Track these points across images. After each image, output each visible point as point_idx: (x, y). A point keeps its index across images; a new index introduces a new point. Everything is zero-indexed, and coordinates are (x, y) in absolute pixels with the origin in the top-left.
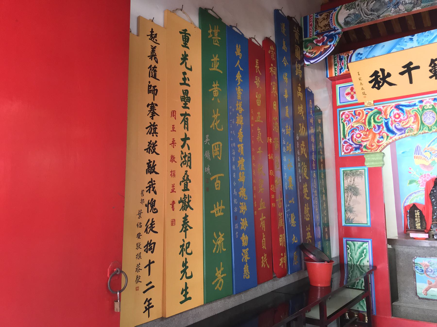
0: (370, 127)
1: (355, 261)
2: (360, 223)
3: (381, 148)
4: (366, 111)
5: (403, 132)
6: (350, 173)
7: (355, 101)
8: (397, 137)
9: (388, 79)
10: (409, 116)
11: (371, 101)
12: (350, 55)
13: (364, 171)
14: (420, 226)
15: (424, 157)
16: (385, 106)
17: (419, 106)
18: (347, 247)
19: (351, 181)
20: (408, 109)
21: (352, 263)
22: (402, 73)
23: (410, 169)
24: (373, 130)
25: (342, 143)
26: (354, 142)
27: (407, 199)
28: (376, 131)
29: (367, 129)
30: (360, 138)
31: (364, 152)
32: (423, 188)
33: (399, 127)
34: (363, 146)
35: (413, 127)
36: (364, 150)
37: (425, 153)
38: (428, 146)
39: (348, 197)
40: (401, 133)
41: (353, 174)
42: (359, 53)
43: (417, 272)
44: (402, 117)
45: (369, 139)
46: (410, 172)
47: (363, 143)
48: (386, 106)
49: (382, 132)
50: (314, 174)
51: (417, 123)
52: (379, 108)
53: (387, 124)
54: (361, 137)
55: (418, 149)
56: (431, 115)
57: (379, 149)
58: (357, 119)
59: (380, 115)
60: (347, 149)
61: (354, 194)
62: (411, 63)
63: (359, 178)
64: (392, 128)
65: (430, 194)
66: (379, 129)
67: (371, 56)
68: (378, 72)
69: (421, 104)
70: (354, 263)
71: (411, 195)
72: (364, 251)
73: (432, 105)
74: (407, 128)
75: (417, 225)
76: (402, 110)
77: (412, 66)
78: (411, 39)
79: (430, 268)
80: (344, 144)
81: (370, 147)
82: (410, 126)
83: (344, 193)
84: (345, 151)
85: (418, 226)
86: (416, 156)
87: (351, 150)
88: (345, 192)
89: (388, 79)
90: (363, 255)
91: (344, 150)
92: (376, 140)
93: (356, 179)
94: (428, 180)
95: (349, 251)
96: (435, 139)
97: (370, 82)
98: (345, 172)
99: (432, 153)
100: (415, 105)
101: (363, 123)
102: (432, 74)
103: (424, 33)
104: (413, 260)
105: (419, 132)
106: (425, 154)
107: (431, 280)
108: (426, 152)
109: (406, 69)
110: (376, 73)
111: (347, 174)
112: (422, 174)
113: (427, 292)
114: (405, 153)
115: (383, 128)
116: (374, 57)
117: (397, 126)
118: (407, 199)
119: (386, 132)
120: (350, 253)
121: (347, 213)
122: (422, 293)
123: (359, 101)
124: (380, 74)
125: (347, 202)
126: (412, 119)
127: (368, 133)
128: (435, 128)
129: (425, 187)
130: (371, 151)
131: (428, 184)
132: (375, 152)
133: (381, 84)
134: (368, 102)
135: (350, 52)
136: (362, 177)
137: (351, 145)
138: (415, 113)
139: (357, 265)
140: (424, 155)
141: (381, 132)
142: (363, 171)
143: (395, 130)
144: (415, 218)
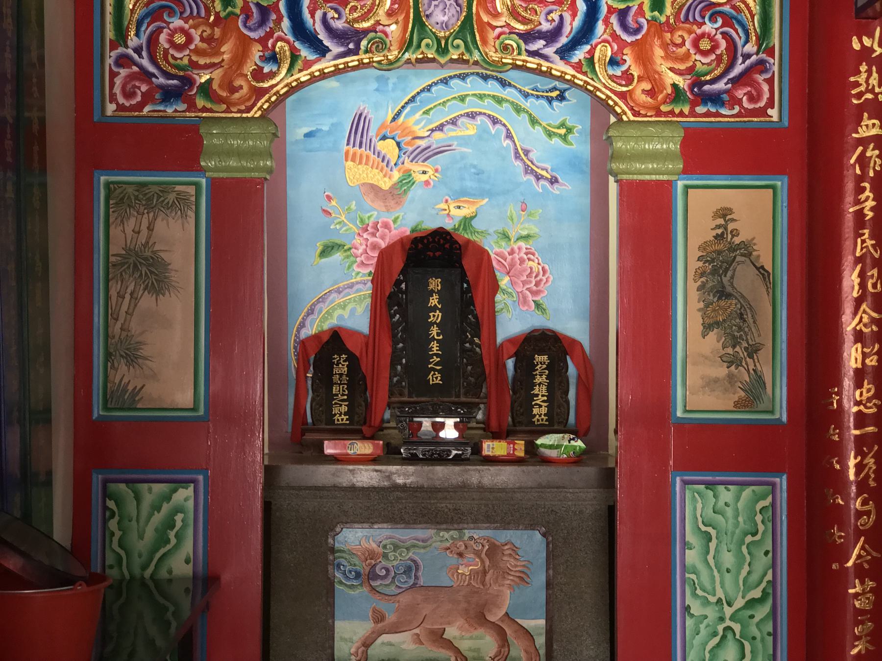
0: (230, 9)
1: (137, 562)
2: (165, 407)
3: (266, 101)
6: (137, 198)
8: (327, 64)
13: (193, 193)
15: (376, 156)
18: (105, 508)
19: (139, 232)
21: (123, 575)
23: (329, 198)
25: (109, 61)
26: (163, 63)
27: (311, 312)
28: (250, 29)
29: (217, 14)
30: (187, 52)
32: (364, 275)
33: (339, 25)
34: (198, 84)
35: (388, 30)
36: (200, 102)
37: (382, 141)
38: (394, 119)
39: (121, 296)
40: (342, 49)
41: (150, 199)
43: (341, 583)
45: (223, 60)
47: (198, 74)
49: (276, 35)
50: (10, 187)
51: (401, 18)
54: (192, 47)
55: (359, 123)
57: (259, 104)
60: (128, 89)
61: (147, 285)
63: (170, 219)
64: (314, 23)
65: (390, 297)
66: (263, 22)
70: (129, 573)
71: (322, 299)
72: (174, 521)
74: (366, 32)
75: (335, 410)
79: (384, 563)
80: (115, 69)
81: (224, 94)
83: (107, 281)
84: (121, 100)
85: (340, 413)
87: (147, 98)
88: (113, 278)
90: (172, 534)
91: (115, 94)
92: (248, 65)
93: (160, 225)
94: (383, 245)
95: (113, 524)
96: (418, 93)
98: (115, 189)
99: (402, 145)
104: (330, 541)
105: (407, 56)
106: (381, 146)
107: (383, 606)
108: (384, 138)
111: (122, 199)
112: (367, 222)
113: (368, 651)
114: (314, 136)
117: (333, 18)
118: (311, 312)
119: (290, 38)
120: (118, 534)
121: (113, 364)
122: (352, 654)
125: (117, 320)
127: (217, 32)
128: (458, 47)
129: (372, 269)
130: (228, 111)
131: (385, 256)
132: (244, 115)
136: (184, 216)
137: (146, 76)
139: (143, 578)
140: (378, 148)
141: (270, 35)
142: (191, 190)
143: (322, 36)
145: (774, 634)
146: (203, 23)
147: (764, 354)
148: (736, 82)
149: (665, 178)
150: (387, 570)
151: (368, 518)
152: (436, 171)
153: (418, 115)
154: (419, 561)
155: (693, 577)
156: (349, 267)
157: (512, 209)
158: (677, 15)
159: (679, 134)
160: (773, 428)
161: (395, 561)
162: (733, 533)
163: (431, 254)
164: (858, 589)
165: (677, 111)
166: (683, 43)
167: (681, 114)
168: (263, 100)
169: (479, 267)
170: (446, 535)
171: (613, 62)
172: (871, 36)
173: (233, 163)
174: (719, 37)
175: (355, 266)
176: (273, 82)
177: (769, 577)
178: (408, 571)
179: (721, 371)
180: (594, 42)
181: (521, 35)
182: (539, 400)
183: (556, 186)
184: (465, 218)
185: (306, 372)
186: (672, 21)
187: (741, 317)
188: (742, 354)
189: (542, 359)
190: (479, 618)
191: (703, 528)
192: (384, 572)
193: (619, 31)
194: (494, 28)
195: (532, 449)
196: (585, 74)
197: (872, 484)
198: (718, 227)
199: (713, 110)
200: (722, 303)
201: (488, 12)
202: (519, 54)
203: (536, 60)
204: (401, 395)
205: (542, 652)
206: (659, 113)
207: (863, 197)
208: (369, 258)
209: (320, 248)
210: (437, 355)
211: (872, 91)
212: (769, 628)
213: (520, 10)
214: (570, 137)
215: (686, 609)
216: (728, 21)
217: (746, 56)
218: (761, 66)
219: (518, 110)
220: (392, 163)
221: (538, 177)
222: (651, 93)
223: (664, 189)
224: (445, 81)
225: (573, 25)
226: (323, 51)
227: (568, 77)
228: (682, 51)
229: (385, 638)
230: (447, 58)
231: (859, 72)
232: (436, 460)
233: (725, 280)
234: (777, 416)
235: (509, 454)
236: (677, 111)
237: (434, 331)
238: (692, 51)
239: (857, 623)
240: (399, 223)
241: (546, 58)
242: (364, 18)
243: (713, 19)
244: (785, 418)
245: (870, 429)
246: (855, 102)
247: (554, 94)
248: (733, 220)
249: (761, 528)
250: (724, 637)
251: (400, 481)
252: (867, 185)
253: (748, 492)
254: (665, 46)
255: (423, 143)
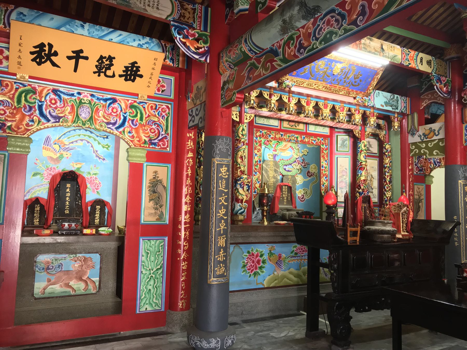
0: (19, 105)
4: (17, 85)
5: (57, 120)
7: (3, 67)
8: (49, 124)
9: (53, 58)
10: (66, 105)
11: (26, 75)
12: (10, 9)
14: (38, 222)
16: (41, 86)
17: (76, 98)
20: (66, 97)
22: (69, 58)
23: (37, 160)
24: (22, 110)
27: (29, 192)
28: (26, 112)
30: (4, 116)
31: (7, 133)
33: (54, 114)
36: (8, 131)
38: (59, 139)
40: (54, 121)
42: (22, 13)
43: (37, 271)
44: (58, 104)
46: (35, 163)
48: (43, 86)
49: (34, 115)
51: (72, 114)
52: (34, 86)
53: (40, 107)
54: (6, 115)
55: (48, 140)
56: (88, 110)
57: (27, 133)
58: (3, 91)
59: (34, 95)
62: (81, 51)
64: (46, 113)
67: (37, 22)
68: (45, 46)
69: (79, 96)
71: (33, 188)
73: (89, 100)
74: (62, 117)
75: (35, 221)
76: (59, 96)
77: (81, 55)
78: (83, 26)
79: (52, 265)
81: (16, 129)
82: (66, 116)
86: (45, 147)
89: (53, 58)
94: (53, 174)
97: (32, 53)
99: (61, 146)
100: (73, 95)
101: (10, 98)
102: (96, 70)
103: (95, 25)
104: (35, 259)
105: (74, 125)
106: (54, 146)
108: (55, 144)
109: (75, 55)
110: (42, 46)
115: (35, 111)
116: (40, 25)
118: (29, 192)
119: (39, 116)
123: (11, 71)
124: (47, 48)
126: (68, 109)
127: (15, 112)
128: (88, 124)
130: (17, 134)
131: (53, 179)
132: (22, 136)
133: (43, 60)
134: (21, 75)
135: (11, 6)
138: (73, 103)
141: (32, 114)
142: (3, 156)
143: (49, 116)
144: (34, 213)
145: (162, 277)
146: (10, 109)
147: (164, 207)
148: (160, 140)
149: (142, 162)
150: (53, 267)
151: (48, 252)
152: (70, 154)
153: (66, 139)
154: (63, 263)
155: (144, 264)
156: (42, 180)
157: (92, 166)
158: (146, 123)
159: (146, 152)
160: (165, 225)
161: (56, 264)
162: (154, 252)
163: (68, 177)
164: (184, 264)
165: (145, 146)
166: (147, 130)
167: (146, 147)
168: (29, 132)
169: (82, 182)
170: (72, 256)
171: (129, 132)
172: (191, 134)
173: (18, 149)
174: (156, 129)
175: (44, 179)
176: (32, 127)
177: (162, 263)
178: (59, 266)
179: (153, 211)
180: (125, 127)
181: (106, 123)
182: (97, 218)
183: (104, 161)
184: (78, 168)
185: (26, 209)
186: (145, 124)
187: (159, 198)
188: (158, 207)
189: (98, 207)
190: (80, 279)
191: (147, 251)
192: (52, 267)
193: (131, 125)
194: (98, 120)
195: (97, 231)
196: (122, 134)
197: (188, 238)
198: (154, 175)
199: (154, 147)
200: (154, 194)
201: (97, 116)
202: (105, 127)
203: (110, 129)
204: (56, 216)
205: (98, 287)
206: (141, 146)
207: (188, 171)
208: (48, 177)
209: (33, 174)
210: (68, 205)
211: (191, 146)
212: (161, 275)
213: (106, 116)
214: (109, 148)
215: (142, 272)
216: (158, 126)
217: (162, 135)
218: (165, 137)
219: (95, 140)
220: (57, 151)
221: (100, 158)
222: (139, 141)
223: (142, 165)
224: (74, 130)
225: (120, 122)
226: (48, 121)
227: (118, 135)
228: (147, 132)
229: (51, 287)
230: (85, 126)
231: (188, 142)
232: (69, 235)
233: (155, 189)
234: (166, 222)
235: (91, 233)
236: (145, 146)
237: (68, 199)
238: (149, 132)
239: (183, 272)
240: (58, 168)
241: (112, 129)
242: (61, 113)
243: (155, 125)
244: (168, 223)
245: (188, 225)
246: (187, 148)
247: (105, 137)
248: (158, 174)
249: (161, 250)
250: (150, 278)
251: (59, 241)
252: (189, 168)
253: (158, 241)
254: (143, 130)
255: (67, 147)
